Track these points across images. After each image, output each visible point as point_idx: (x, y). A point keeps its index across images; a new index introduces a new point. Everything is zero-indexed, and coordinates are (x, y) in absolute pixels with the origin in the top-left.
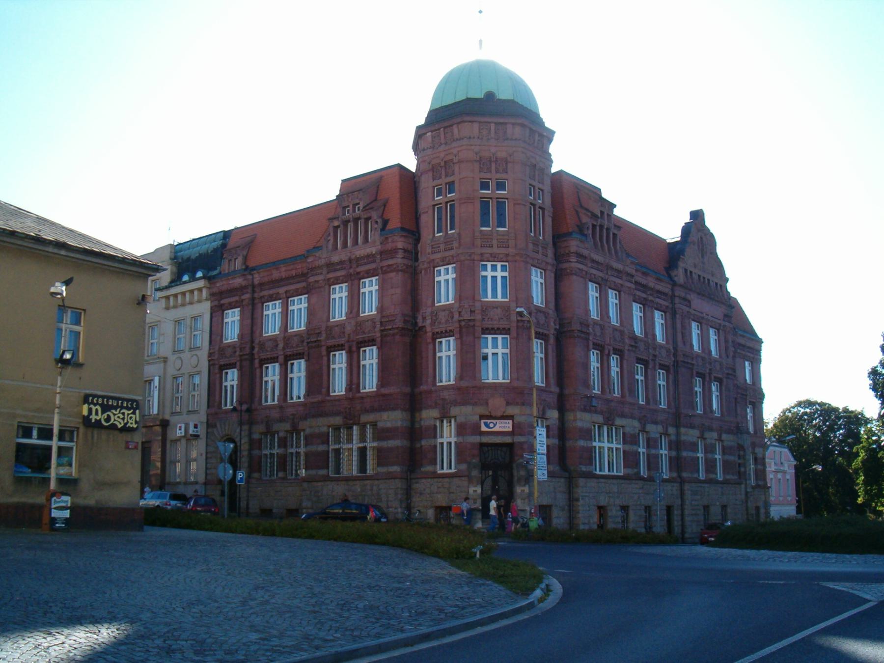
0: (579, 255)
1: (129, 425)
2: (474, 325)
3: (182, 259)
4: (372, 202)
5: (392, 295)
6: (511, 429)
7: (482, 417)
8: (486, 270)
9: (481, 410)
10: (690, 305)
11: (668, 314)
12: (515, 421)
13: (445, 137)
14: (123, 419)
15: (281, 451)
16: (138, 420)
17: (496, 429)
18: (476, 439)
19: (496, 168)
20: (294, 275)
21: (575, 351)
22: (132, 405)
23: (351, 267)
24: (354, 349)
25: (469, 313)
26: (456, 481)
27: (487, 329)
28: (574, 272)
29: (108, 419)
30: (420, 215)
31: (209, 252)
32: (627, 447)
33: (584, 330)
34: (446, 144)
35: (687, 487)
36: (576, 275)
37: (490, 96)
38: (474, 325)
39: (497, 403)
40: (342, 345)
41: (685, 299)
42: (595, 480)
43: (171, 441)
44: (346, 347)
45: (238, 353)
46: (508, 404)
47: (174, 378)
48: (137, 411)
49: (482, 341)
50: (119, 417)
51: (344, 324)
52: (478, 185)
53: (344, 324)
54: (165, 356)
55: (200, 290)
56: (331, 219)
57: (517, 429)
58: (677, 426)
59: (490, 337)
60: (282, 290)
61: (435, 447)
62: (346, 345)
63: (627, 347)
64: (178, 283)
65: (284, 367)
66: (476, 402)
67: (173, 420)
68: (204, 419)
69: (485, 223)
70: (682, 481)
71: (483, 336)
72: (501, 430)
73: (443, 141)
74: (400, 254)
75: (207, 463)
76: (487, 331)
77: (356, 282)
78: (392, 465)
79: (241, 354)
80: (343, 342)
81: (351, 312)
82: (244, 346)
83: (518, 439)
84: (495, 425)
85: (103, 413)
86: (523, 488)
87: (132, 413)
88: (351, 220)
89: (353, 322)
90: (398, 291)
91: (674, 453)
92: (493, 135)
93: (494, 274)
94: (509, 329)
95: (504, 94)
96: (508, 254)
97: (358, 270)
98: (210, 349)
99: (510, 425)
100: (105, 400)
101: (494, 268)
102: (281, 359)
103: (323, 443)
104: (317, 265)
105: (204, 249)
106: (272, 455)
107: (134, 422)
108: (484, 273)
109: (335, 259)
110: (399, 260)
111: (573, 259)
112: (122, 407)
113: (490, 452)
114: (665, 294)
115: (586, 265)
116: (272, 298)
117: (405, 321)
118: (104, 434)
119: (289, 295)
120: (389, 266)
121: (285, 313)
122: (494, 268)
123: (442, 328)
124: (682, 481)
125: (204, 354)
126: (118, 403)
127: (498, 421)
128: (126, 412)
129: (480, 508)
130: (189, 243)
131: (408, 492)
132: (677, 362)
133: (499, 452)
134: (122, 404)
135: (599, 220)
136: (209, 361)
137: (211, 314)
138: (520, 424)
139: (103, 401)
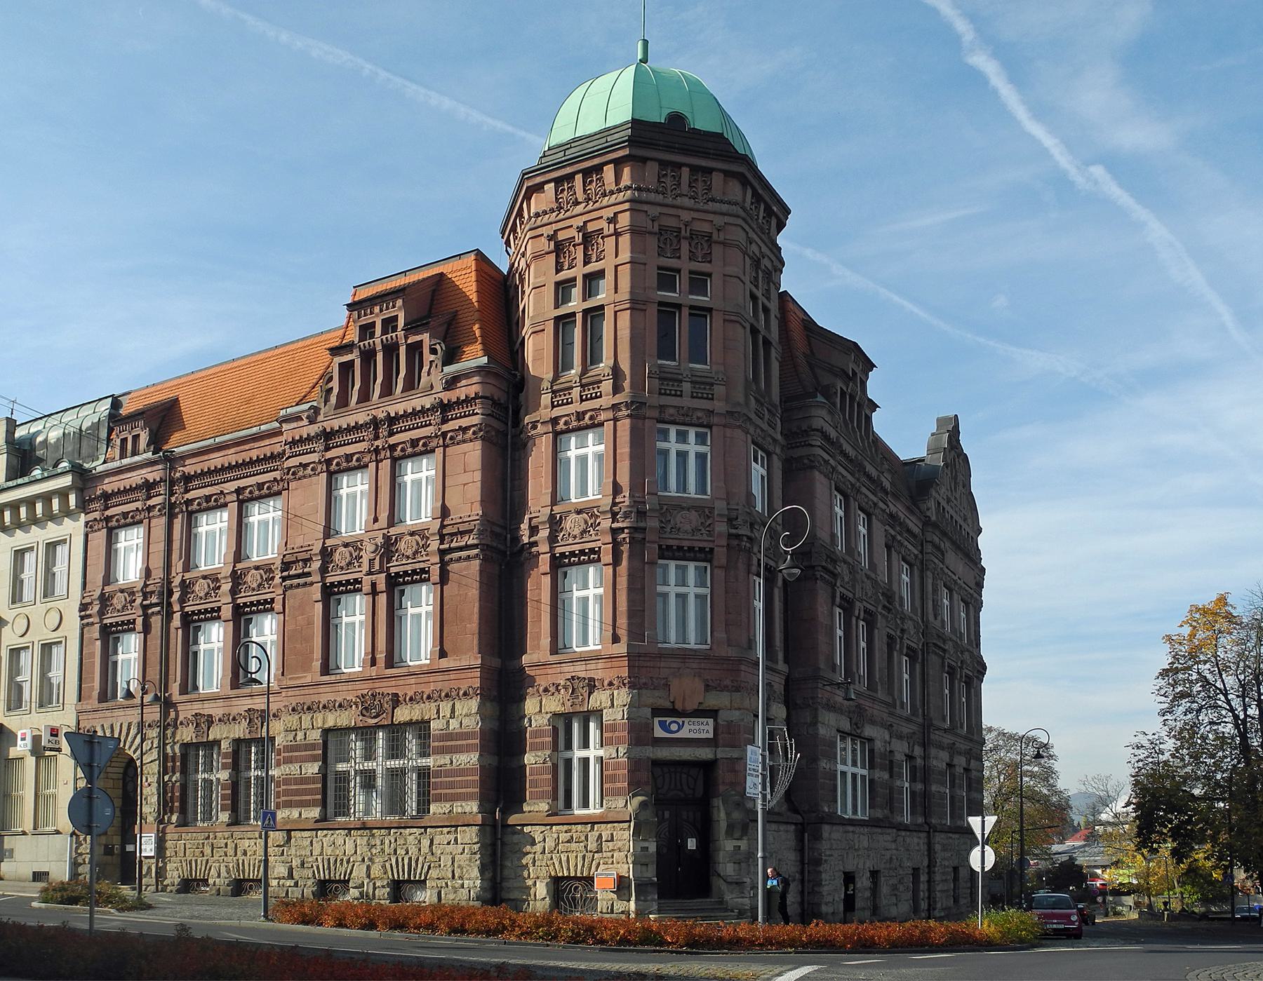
0: (826, 437)
5: (465, 485)
6: (711, 735)
7: (657, 712)
8: (666, 439)
10: (943, 559)
12: (719, 721)
17: (683, 734)
23: (377, 438)
24: (382, 586)
27: (669, 547)
33: (830, 567)
35: (939, 838)
37: (676, 119)
41: (938, 548)
42: (841, 828)
44: (367, 587)
45: (139, 601)
49: (659, 571)
55: (63, 494)
56: (335, 351)
59: (672, 564)
71: (660, 561)
72: (692, 735)
73: (581, 196)
81: (376, 520)
83: (722, 753)
88: (379, 347)
90: (478, 476)
91: (919, 786)
92: (685, 187)
93: (682, 447)
94: (712, 550)
95: (702, 122)
96: (712, 412)
101: (682, 437)
102: (227, 612)
108: (661, 445)
114: (914, 536)
119: (244, 501)
122: (682, 437)
127: (686, 720)
129: (656, 879)
133: (684, 776)
138: (730, 724)
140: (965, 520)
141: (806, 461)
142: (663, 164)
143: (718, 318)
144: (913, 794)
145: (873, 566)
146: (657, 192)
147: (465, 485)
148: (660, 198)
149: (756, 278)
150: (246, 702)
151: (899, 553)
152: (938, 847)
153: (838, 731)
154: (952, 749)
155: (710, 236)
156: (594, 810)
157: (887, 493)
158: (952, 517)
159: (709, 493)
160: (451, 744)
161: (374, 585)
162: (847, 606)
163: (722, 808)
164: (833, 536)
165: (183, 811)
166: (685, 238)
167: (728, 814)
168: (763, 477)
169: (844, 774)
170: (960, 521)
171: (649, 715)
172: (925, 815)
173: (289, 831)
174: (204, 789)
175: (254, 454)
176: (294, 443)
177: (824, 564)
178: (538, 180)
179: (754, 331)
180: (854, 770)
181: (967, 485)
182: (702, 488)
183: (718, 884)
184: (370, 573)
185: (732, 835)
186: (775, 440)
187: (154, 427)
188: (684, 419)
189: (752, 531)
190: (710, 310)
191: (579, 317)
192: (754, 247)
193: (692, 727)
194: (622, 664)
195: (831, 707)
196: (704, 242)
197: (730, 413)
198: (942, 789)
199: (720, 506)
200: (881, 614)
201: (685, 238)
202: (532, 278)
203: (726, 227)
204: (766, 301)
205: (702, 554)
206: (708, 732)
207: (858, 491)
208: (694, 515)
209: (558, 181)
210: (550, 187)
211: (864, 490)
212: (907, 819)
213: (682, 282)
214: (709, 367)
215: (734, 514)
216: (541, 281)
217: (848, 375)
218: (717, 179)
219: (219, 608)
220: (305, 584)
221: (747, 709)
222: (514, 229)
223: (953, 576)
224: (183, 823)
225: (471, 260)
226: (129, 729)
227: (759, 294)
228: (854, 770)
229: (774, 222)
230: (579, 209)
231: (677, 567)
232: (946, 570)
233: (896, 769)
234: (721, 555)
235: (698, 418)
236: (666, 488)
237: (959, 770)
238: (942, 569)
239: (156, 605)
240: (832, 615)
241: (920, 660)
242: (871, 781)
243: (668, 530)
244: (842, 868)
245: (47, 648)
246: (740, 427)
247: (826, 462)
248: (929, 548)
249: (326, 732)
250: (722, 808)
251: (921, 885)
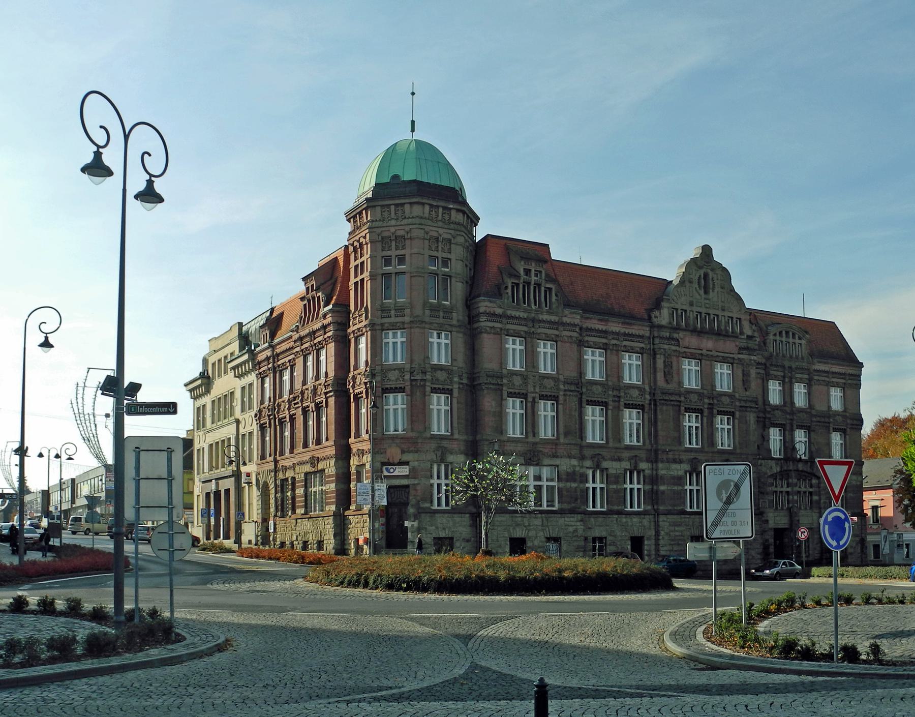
7: (383, 464)
11: (645, 355)
13: (396, 214)
17: (396, 473)
19: (396, 245)
21: (488, 402)
32: (562, 485)
36: (485, 333)
42: (507, 516)
46: (403, 452)
57: (413, 474)
63: (562, 393)
84: (394, 470)
86: (413, 523)
94: (452, 390)
101: (395, 336)
111: (483, 319)
113: (396, 492)
122: (395, 336)
132: (655, 400)
133: (403, 492)
155: (450, 240)
165: (282, 511)
173: (296, 519)
187: (273, 328)
188: (394, 327)
194: (332, 449)
196: (400, 240)
199: (408, 366)
213: (394, 261)
218: (453, 213)
224: (283, 516)
230: (393, 222)
234: (408, 389)
235: (435, 327)
249: (306, 474)
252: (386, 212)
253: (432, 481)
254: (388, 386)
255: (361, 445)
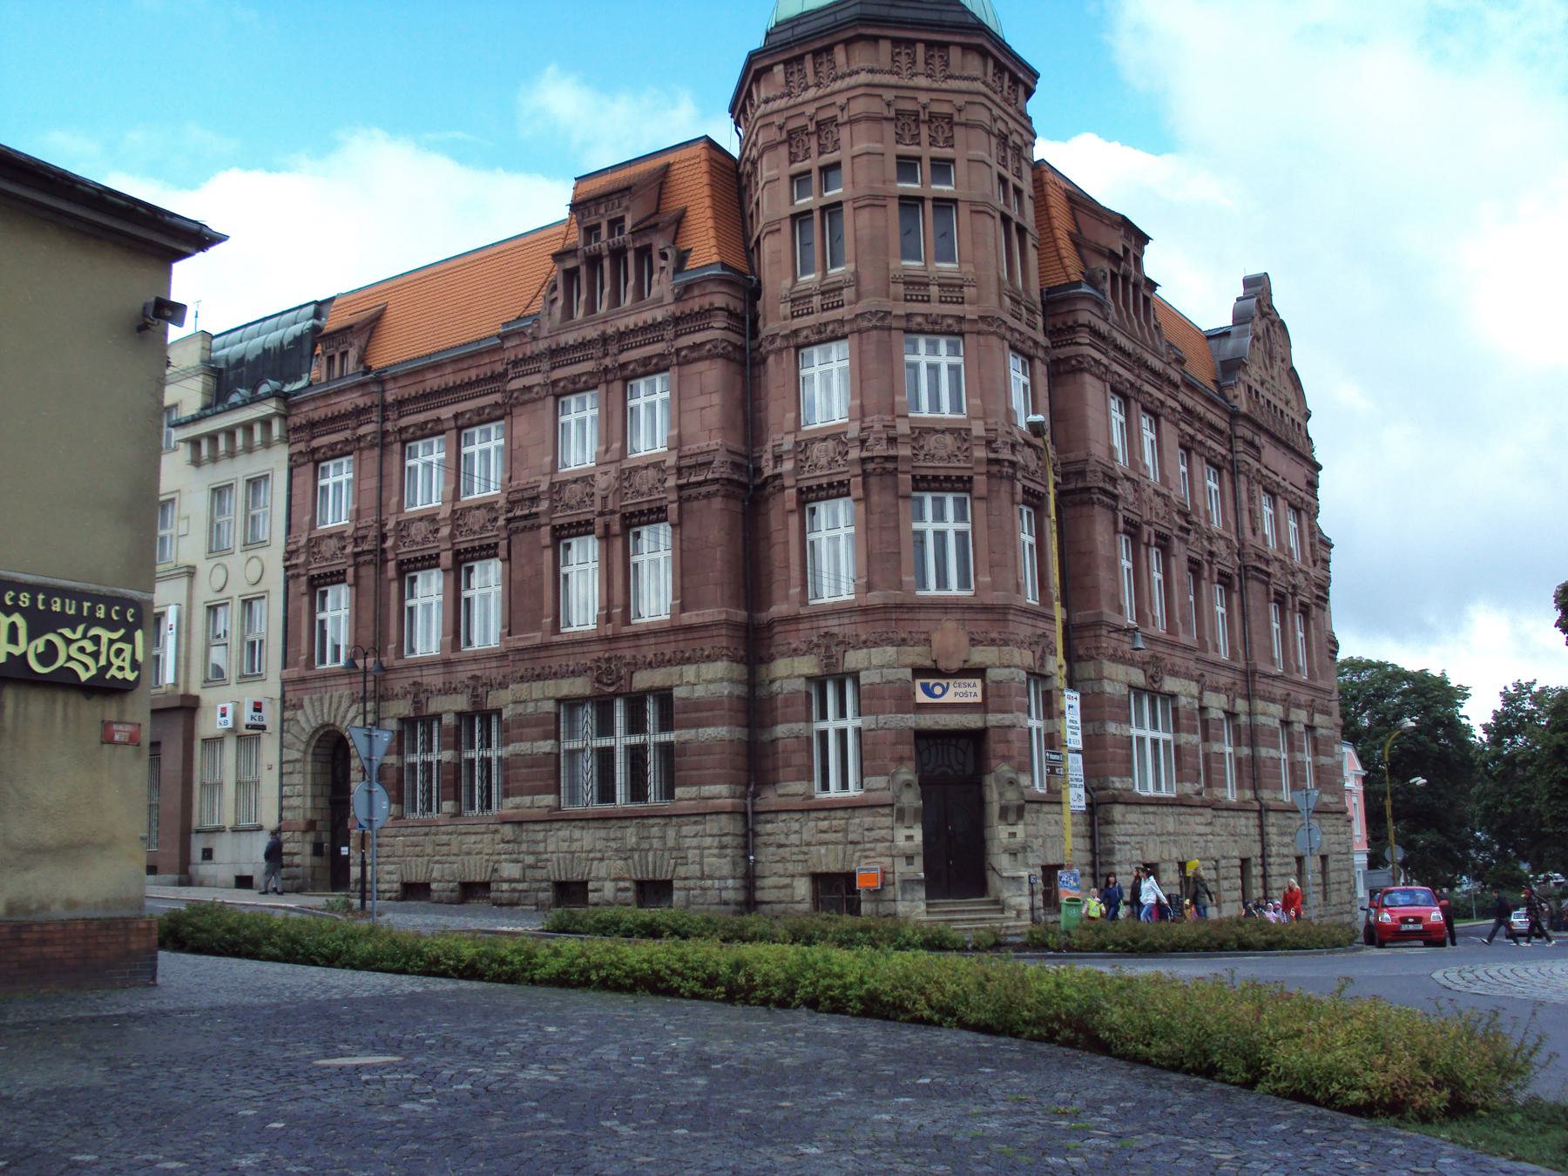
0: (1095, 332)
1: (113, 672)
2: (896, 469)
3: (227, 361)
4: (652, 216)
5: (703, 408)
6: (979, 699)
7: (919, 672)
9: (916, 655)
12: (988, 681)
13: (816, 73)
14: (95, 655)
15: (447, 756)
16: (140, 657)
18: (912, 720)
19: (820, 145)
20: (474, 378)
22: (122, 614)
23: (606, 355)
24: (616, 528)
25: (884, 442)
26: (866, 819)
27: (924, 478)
28: (1086, 365)
29: (49, 655)
30: (758, 242)
31: (285, 343)
33: (1109, 487)
34: (818, 85)
35: (1272, 818)
38: (896, 469)
39: (950, 640)
40: (589, 523)
41: (1251, 444)
43: (204, 740)
44: (599, 529)
45: (349, 549)
46: (974, 642)
47: (209, 607)
48: (139, 635)
50: (82, 650)
51: (593, 476)
52: (891, 166)
53: (593, 476)
54: (191, 563)
55: (266, 422)
56: (558, 257)
58: (1248, 697)
59: (928, 499)
60: (446, 413)
61: (809, 740)
62: (597, 520)
64: (219, 408)
65: (452, 575)
66: (904, 640)
67: (208, 696)
68: (277, 694)
69: (910, 252)
70: (1262, 811)
74: (719, 322)
75: (281, 785)
76: (924, 483)
77: (618, 386)
78: (714, 781)
79: (356, 550)
80: (589, 516)
82: (361, 533)
83: (994, 719)
84: (945, 691)
85: (32, 637)
87: (121, 639)
88: (605, 253)
89: (612, 469)
90: (716, 399)
91: (1245, 751)
97: (623, 358)
98: (287, 544)
99: (978, 689)
100: (41, 597)
102: (446, 559)
103: (546, 737)
104: (529, 354)
105: (273, 338)
106: (428, 766)
107: (127, 665)
109: (569, 338)
110: (715, 332)
112: (92, 621)
114: (1220, 432)
115: (1105, 354)
116: (427, 431)
117: (736, 466)
118: (36, 704)
119: (461, 426)
120: (696, 347)
121: (453, 464)
123: (821, 477)
124: (1262, 811)
125: (273, 559)
126: (80, 608)
127: (951, 681)
128: (105, 635)
129: (922, 875)
130: (240, 332)
131: (748, 841)
133: (952, 749)
134: (92, 610)
135: (1123, 264)
136: (287, 568)
137: (291, 470)
139: (34, 600)
140: (1287, 403)
141: (1074, 362)
142: (896, 42)
143: (964, 210)
144: (1239, 761)
145: (1164, 479)
146: (891, 72)
147: (703, 408)
148: (892, 80)
149: (1004, 158)
150: (469, 668)
151: (1201, 455)
152: (1272, 830)
153: (1130, 686)
154: (1287, 702)
155: (950, 117)
156: (853, 792)
157: (1176, 387)
158: (1269, 402)
159: (965, 411)
160: (700, 712)
161: (607, 526)
162: (1133, 530)
163: (994, 786)
164: (1111, 449)
166: (924, 122)
167: (1001, 795)
168: (1025, 386)
169: (1141, 740)
170: (1281, 405)
171: (910, 677)
172: (1255, 789)
174: (423, 772)
175: (473, 374)
176: (516, 363)
177: (1101, 485)
178: (767, 62)
179: (1006, 219)
180: (1155, 735)
181: (1287, 359)
182: (956, 407)
183: (993, 880)
184: (601, 514)
185: (1006, 819)
186: (1036, 343)
188: (933, 328)
189: (1013, 453)
190: (955, 201)
191: (817, 215)
192: (1000, 125)
193: (959, 690)
195: (1117, 658)
197: (982, 318)
198: (1273, 753)
199: (854, 431)
200: (1177, 537)
201: (924, 122)
202: (765, 171)
203: (968, 107)
204: (1017, 182)
205: (961, 484)
206: (975, 695)
207: (1139, 390)
208: (948, 439)
209: (786, 63)
210: (778, 69)
211: (1147, 388)
212: (1231, 794)
214: (956, 266)
215: (992, 435)
216: (774, 172)
217: (1117, 255)
218: (955, 54)
219: (438, 555)
220: (532, 528)
221: (1017, 667)
222: (743, 110)
223: (1274, 477)
225: (699, 149)
226: (340, 702)
227: (1008, 174)
228: (1155, 735)
229: (1021, 90)
230: (811, 93)
231: (934, 499)
232: (1265, 472)
233: (1212, 731)
234: (981, 484)
235: (949, 326)
236: (917, 408)
237: (1298, 728)
238: (1258, 470)
239: (370, 552)
240: (1115, 545)
241: (1237, 588)
242: (1177, 747)
243: (922, 457)
244: (1140, 859)
245: (247, 603)
246: (994, 333)
247: (1097, 362)
248: (1240, 446)
250: (994, 786)
251: (1254, 881)
252: (796, 76)
253: (858, 722)
254: (813, 483)
255: (836, 622)
